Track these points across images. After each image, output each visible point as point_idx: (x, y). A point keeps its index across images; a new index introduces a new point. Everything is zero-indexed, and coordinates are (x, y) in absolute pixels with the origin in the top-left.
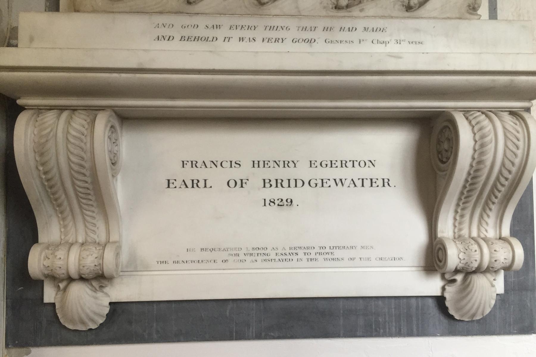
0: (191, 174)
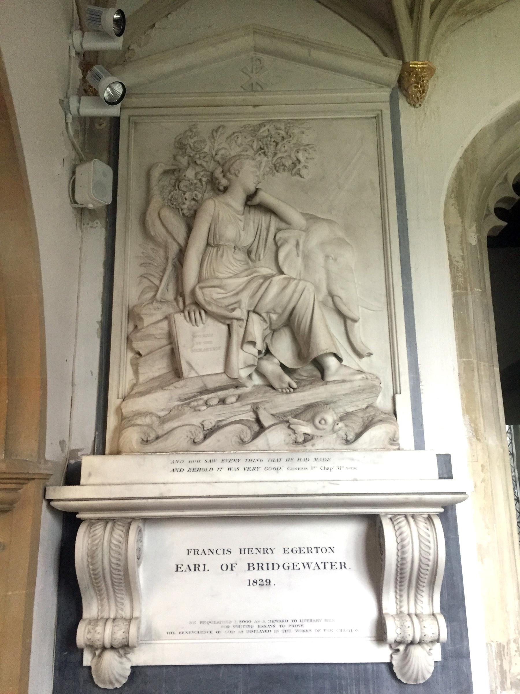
0: (194, 560)
